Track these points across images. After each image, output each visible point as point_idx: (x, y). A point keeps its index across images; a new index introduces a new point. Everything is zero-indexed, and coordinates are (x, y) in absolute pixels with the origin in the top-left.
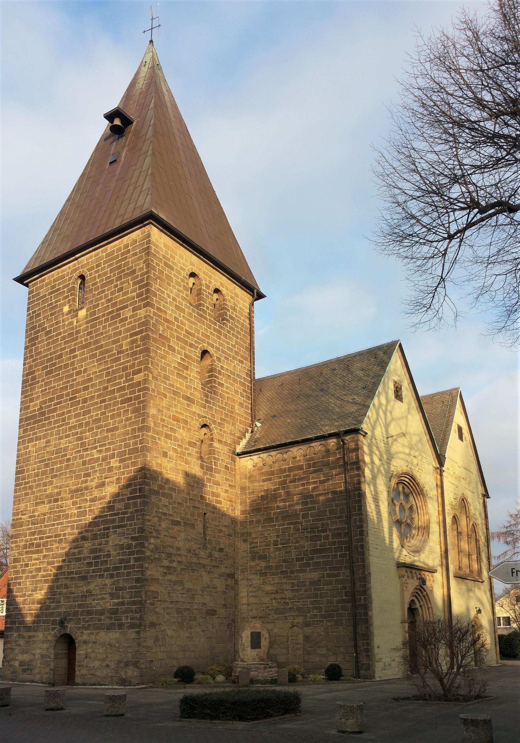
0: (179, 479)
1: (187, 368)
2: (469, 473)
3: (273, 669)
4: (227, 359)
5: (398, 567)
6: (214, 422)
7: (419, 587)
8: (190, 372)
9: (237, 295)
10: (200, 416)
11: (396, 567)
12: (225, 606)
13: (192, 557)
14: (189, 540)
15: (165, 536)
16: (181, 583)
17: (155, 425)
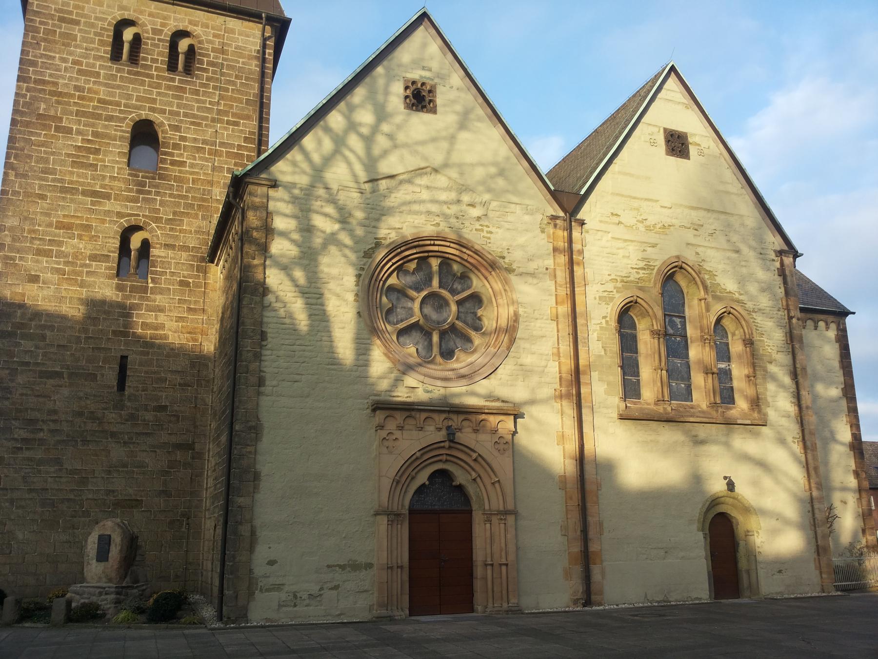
0: (73, 310)
1: (97, 151)
2: (723, 217)
3: (108, 596)
4: (199, 124)
5: (374, 410)
6: (157, 220)
7: (447, 444)
8: (104, 155)
9: (232, 31)
10: (120, 215)
11: (369, 411)
12: (165, 493)
13: (85, 423)
14: (80, 398)
15: (22, 395)
16: (58, 462)
17: (14, 240)
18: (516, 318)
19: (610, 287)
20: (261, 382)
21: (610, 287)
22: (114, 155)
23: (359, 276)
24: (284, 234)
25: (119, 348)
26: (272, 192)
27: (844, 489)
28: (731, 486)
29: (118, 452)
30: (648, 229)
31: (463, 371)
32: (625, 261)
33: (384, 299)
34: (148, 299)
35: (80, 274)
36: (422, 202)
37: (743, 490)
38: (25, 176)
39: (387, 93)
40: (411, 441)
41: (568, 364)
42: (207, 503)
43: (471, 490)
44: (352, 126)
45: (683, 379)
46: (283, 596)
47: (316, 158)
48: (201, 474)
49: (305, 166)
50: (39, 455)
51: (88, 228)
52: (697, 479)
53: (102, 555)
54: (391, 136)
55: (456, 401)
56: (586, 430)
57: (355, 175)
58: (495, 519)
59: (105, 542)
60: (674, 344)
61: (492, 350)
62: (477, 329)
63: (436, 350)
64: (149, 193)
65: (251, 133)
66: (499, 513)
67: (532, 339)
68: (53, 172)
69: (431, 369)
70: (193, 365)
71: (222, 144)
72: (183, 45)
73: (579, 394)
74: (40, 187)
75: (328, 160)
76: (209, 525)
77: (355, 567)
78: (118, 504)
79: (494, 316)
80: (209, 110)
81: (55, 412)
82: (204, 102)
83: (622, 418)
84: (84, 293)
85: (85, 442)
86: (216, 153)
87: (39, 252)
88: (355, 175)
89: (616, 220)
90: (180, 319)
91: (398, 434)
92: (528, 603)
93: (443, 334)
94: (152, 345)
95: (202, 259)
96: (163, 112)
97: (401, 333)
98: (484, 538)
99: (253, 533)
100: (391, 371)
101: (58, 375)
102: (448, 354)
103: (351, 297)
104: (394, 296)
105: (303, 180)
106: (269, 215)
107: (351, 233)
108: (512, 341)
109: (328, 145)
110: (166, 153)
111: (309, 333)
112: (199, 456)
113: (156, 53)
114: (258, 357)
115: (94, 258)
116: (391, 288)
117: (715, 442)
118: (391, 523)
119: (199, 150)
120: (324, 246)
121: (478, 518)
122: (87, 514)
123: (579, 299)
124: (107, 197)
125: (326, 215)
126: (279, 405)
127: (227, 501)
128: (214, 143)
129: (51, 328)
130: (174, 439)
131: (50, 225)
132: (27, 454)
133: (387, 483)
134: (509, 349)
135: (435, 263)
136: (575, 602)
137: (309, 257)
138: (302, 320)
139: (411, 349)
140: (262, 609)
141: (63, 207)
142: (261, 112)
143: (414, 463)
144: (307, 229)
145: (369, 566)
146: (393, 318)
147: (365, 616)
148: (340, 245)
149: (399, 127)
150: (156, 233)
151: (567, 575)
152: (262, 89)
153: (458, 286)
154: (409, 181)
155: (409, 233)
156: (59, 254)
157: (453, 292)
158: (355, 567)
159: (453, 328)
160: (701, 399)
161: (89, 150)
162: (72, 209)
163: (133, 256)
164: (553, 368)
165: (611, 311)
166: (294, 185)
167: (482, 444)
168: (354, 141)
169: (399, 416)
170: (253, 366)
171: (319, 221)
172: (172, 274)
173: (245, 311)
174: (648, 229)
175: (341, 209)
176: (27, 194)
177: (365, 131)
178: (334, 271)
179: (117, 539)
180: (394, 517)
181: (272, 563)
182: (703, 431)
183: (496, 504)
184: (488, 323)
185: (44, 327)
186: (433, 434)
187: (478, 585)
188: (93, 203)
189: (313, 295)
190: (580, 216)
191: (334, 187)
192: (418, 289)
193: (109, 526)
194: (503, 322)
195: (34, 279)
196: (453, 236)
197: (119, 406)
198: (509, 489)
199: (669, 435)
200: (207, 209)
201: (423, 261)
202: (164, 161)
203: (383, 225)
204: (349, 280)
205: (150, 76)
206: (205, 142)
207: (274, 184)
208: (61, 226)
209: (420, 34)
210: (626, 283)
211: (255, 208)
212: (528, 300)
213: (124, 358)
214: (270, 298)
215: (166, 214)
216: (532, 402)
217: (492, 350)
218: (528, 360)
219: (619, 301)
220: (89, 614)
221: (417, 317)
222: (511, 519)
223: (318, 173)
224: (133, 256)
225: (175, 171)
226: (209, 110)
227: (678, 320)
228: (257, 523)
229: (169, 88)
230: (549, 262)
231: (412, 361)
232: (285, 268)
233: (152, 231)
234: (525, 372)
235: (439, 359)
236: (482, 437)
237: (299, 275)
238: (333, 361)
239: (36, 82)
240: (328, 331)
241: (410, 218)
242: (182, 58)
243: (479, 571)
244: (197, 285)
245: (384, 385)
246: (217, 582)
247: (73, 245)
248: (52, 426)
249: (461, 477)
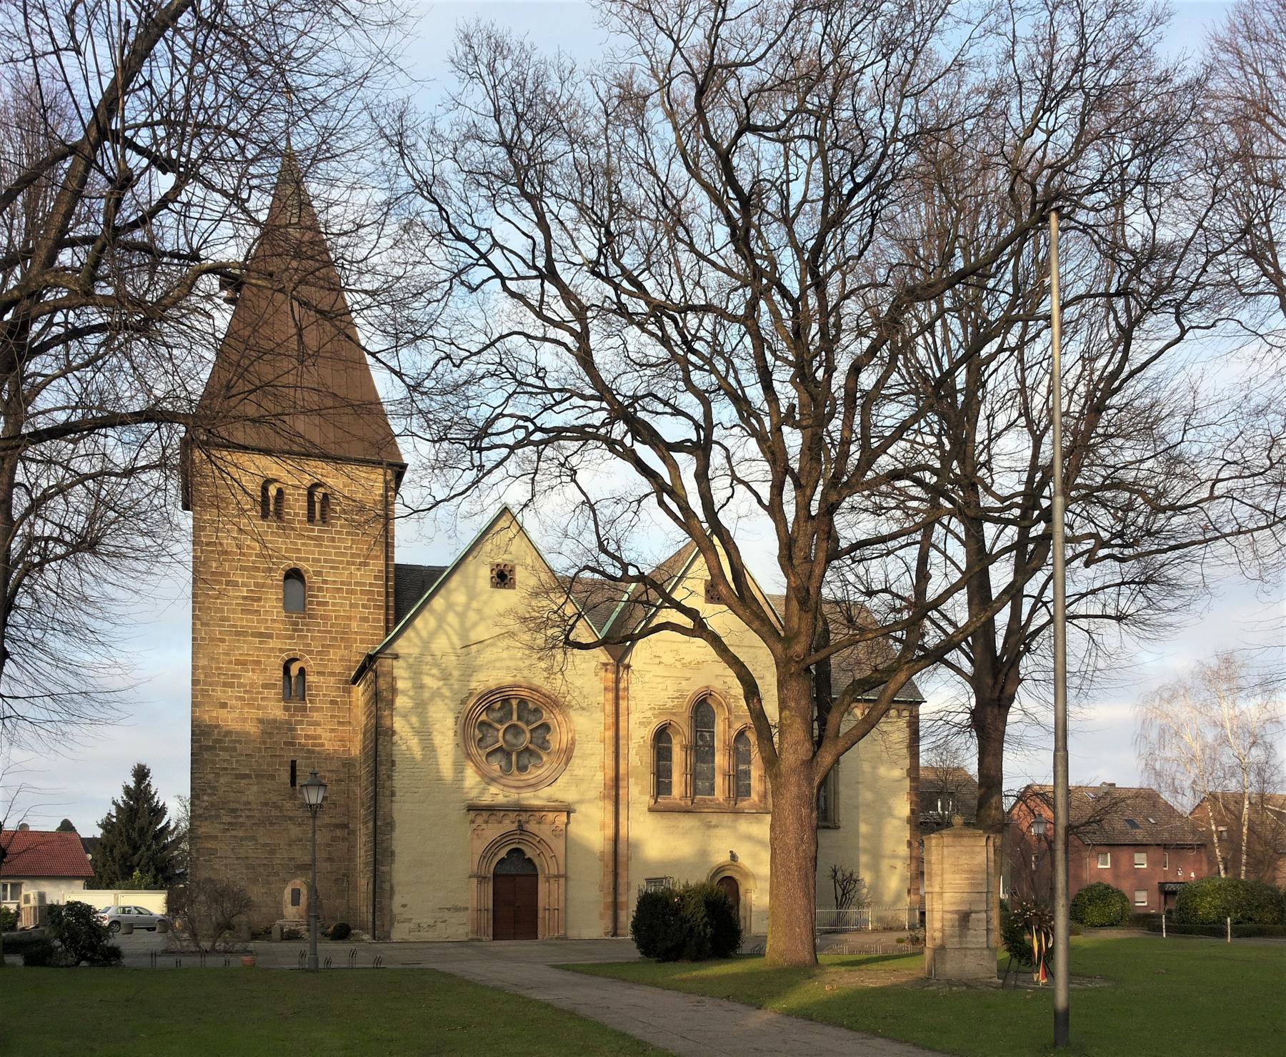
0: (252, 728)
1: (259, 599)
4: (337, 568)
10: (281, 650)
16: (254, 838)
18: (573, 742)
19: (649, 714)
20: (393, 794)
21: (649, 714)
22: (272, 603)
23: (457, 718)
24: (404, 693)
25: (289, 755)
26: (395, 663)
27: (894, 856)
28: (733, 857)
29: (295, 831)
30: (684, 665)
31: (532, 781)
32: (663, 693)
33: (477, 731)
34: (307, 716)
35: (256, 700)
36: (503, 660)
37: (744, 860)
38: (207, 625)
39: (476, 577)
40: (493, 831)
41: (611, 773)
42: (360, 867)
43: (536, 861)
44: (450, 606)
45: (707, 779)
46: (412, 926)
47: (424, 634)
48: (355, 846)
49: (416, 641)
50: (241, 834)
51: (258, 663)
52: (704, 854)
53: (295, 902)
54: (479, 611)
55: (525, 802)
56: (622, 819)
57: (452, 644)
58: (552, 881)
59: (296, 894)
60: (701, 751)
61: (555, 765)
62: (545, 749)
63: (514, 767)
64: (302, 630)
65: (380, 571)
66: (555, 876)
67: (584, 757)
68: (227, 619)
69: (509, 781)
70: (344, 765)
71: (357, 584)
72: (319, 493)
73: (617, 795)
74: (220, 632)
75: (432, 635)
76: (363, 882)
77: (457, 909)
78: (298, 867)
79: (558, 739)
80: (344, 554)
81: (249, 803)
82: (339, 548)
83: (651, 810)
84: (260, 714)
85: (272, 824)
86: (351, 592)
87: (225, 685)
88: (452, 644)
89: (657, 660)
90: (332, 730)
91: (484, 826)
92: (573, 934)
93: (519, 754)
94: (313, 752)
95: (346, 682)
96: (307, 560)
97: (489, 755)
98: (546, 893)
99: (392, 888)
100: (479, 783)
101: (248, 776)
102: (523, 769)
103: (451, 733)
104: (484, 728)
105: (415, 651)
106: (394, 678)
107: (450, 687)
108: (568, 760)
109: (432, 623)
110: (312, 596)
111: (423, 760)
112: (352, 833)
113: (297, 506)
114: (390, 777)
115: (265, 686)
116: (483, 723)
117: (725, 827)
118: (480, 883)
119: (339, 590)
120: (432, 697)
121: (541, 879)
122: (277, 874)
123: (622, 724)
124: (270, 636)
125: (433, 676)
126: (405, 809)
128: (350, 584)
129: (240, 742)
130: (334, 821)
131: (230, 663)
132: (233, 833)
133: (477, 858)
134: (566, 764)
135: (514, 703)
136: (606, 934)
137: (421, 706)
138: (418, 753)
139: (495, 766)
140: (399, 932)
141: (239, 648)
142: (387, 552)
143: (495, 845)
144: (420, 687)
145: (466, 909)
146: (482, 744)
147: (463, 938)
148: (443, 697)
149: (485, 603)
150: (310, 663)
151: (602, 916)
152: (386, 530)
153: (532, 718)
154: (493, 645)
155: (492, 684)
156: (240, 685)
157: (528, 723)
158: (457, 909)
159: (527, 749)
160: (720, 793)
161: (252, 599)
162: (245, 648)
163: (294, 683)
164: (599, 777)
165: (647, 733)
166: (410, 655)
167: (544, 831)
168: (452, 618)
169: (485, 815)
170: (387, 784)
171: (428, 681)
172: (325, 695)
173: (380, 748)
174: (684, 665)
175: (443, 671)
176: (212, 639)
177: (459, 609)
178: (440, 715)
179: (304, 891)
180: (481, 879)
181: (404, 906)
182: (714, 819)
183: (554, 871)
184: (554, 745)
185: (235, 741)
186: (508, 825)
187: (540, 922)
188: (260, 643)
189: (425, 734)
190: (626, 661)
191: (439, 654)
192: (501, 721)
193: (298, 883)
194: (564, 745)
195: (224, 705)
196: (525, 684)
197: (293, 797)
198: (562, 862)
199: (687, 822)
200: (347, 640)
201: (506, 701)
202: (311, 603)
203: (474, 678)
204: (450, 721)
205: (293, 529)
206: (342, 583)
207: (396, 657)
208: (238, 662)
209: (503, 523)
210: (663, 710)
211: (385, 675)
212: (584, 728)
213: (294, 762)
214: (396, 738)
215: (316, 647)
216: (581, 802)
217: (555, 765)
218: (580, 772)
219: (655, 725)
220: (292, 936)
221: (501, 743)
222: (562, 881)
223: (426, 644)
224: (294, 683)
225: (320, 611)
226: (344, 554)
227: (707, 735)
228: (395, 881)
229: (310, 538)
230: (601, 699)
231: (495, 775)
232: (405, 716)
233: (307, 661)
234: (578, 781)
235: (516, 772)
236: (542, 826)
237: (414, 720)
238: (440, 779)
239: (208, 544)
240: (435, 757)
241: (494, 673)
242: (320, 506)
243: (540, 914)
244: (344, 703)
245: (474, 793)
246: (371, 918)
247: (249, 677)
248: (248, 813)
249: (529, 853)
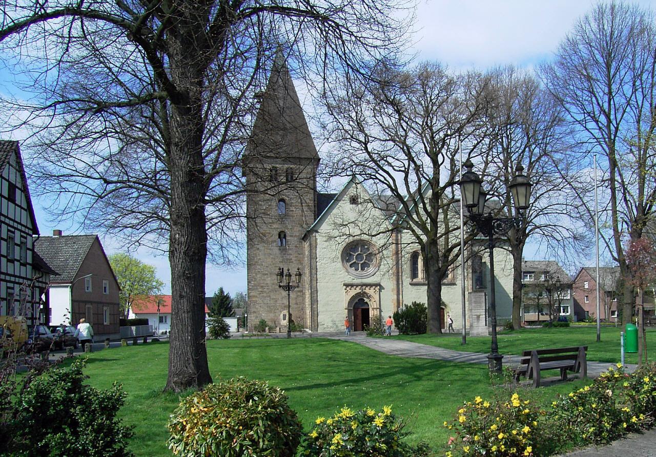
16: (270, 296)
40: (353, 292)
42: (307, 306)
53: (284, 319)
59: (284, 316)
101: (267, 274)
112: (304, 294)
122: (278, 309)
127: (311, 307)
186: (358, 290)
